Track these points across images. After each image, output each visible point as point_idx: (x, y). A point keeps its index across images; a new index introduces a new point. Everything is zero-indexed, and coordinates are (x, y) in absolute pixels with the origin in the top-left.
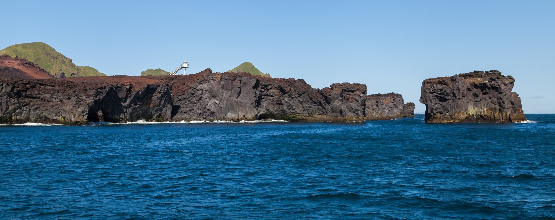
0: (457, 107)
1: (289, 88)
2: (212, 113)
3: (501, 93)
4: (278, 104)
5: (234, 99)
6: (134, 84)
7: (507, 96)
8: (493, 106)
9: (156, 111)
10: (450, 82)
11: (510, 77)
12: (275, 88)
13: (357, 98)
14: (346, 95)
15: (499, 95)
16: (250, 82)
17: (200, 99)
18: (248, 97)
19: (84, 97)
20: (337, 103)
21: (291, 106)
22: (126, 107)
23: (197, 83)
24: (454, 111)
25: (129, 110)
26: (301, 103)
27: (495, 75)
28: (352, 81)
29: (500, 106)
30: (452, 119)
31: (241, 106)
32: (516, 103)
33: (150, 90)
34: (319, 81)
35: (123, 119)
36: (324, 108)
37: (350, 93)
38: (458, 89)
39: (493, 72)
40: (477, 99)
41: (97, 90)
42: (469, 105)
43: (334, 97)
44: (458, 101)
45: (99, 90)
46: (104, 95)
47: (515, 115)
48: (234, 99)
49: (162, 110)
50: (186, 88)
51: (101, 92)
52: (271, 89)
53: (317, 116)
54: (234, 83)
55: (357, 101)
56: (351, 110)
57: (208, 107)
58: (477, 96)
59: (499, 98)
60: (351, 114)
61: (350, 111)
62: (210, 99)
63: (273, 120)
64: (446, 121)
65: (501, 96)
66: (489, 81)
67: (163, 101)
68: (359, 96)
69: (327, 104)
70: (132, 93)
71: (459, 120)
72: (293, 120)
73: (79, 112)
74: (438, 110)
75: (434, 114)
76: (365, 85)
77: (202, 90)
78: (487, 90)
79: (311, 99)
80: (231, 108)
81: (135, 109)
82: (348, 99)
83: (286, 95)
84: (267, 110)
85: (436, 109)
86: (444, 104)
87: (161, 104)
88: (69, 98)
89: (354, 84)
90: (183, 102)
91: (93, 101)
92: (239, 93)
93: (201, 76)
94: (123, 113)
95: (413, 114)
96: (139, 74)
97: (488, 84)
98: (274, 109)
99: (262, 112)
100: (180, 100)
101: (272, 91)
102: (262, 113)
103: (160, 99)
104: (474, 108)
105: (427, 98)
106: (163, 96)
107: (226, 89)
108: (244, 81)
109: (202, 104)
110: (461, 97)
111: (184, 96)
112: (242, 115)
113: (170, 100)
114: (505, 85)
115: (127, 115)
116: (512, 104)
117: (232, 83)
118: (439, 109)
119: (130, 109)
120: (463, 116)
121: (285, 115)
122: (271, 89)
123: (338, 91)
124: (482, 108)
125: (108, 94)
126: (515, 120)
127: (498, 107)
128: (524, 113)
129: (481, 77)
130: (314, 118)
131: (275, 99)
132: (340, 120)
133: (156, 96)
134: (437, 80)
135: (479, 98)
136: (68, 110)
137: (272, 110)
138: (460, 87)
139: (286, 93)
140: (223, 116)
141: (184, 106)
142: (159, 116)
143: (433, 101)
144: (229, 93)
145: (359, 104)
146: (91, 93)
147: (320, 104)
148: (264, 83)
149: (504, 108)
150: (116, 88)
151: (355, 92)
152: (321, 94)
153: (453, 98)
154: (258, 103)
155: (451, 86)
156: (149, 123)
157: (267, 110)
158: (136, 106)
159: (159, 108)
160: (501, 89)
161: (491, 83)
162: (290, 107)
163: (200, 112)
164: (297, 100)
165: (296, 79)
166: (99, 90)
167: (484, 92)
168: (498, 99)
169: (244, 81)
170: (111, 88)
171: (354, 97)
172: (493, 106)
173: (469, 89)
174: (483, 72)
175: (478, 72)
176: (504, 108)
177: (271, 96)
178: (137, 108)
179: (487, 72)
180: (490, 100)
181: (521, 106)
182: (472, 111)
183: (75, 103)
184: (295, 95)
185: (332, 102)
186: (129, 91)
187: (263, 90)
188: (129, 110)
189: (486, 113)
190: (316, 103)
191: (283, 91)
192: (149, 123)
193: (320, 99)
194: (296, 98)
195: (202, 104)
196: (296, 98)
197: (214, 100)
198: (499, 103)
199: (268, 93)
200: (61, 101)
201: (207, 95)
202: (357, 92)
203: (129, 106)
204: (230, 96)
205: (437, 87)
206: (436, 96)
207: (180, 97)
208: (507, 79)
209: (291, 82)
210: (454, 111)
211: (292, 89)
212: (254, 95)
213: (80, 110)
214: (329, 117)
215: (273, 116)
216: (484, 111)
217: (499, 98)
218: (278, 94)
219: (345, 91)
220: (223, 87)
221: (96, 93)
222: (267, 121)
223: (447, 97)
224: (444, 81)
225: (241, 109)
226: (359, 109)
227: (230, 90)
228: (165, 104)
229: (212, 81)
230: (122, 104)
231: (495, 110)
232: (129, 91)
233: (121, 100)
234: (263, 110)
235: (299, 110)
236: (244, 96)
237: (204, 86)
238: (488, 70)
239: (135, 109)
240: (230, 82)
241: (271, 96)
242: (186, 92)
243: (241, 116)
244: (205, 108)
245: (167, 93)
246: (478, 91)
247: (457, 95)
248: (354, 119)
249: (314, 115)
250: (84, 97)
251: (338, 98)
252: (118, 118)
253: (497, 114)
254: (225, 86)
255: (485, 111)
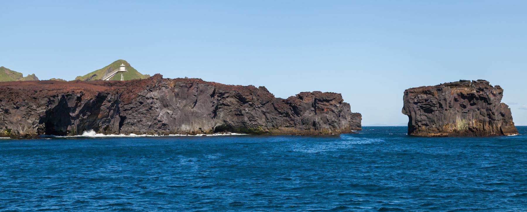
0: (445, 119)
1: (250, 97)
2: (164, 125)
3: (490, 104)
4: (236, 115)
5: (189, 109)
6: (84, 92)
7: (496, 107)
8: (482, 118)
9: (103, 123)
10: (435, 92)
11: (498, 87)
12: (232, 97)
13: (333, 109)
14: (320, 105)
15: (488, 106)
16: (207, 89)
17: (150, 109)
18: (204, 108)
19: (34, 107)
20: (308, 114)
21: (253, 117)
22: (74, 118)
23: (146, 91)
24: (441, 123)
25: (77, 122)
26: (264, 113)
27: (482, 85)
28: (191, 76)
29: (490, 118)
30: (440, 132)
31: (197, 117)
32: (506, 115)
33: (101, 98)
34: (282, 91)
35: (70, 132)
36: (292, 120)
37: (325, 103)
38: (445, 100)
39: (481, 82)
40: (465, 110)
41: (49, 99)
42: (457, 117)
43: (305, 108)
44: (444, 112)
45: (52, 99)
46: (56, 104)
47: (507, 127)
48: (189, 109)
49: (109, 122)
50: (134, 96)
51: (53, 101)
52: (227, 97)
53: (283, 128)
54: (190, 91)
55: (333, 111)
56: (327, 121)
57: (159, 119)
58: (464, 107)
59: (488, 110)
60: (327, 127)
61: (325, 123)
62: (161, 109)
63: (233, 134)
64: (433, 134)
65: (491, 107)
66: (477, 92)
67: (112, 111)
68: (335, 106)
69: (295, 115)
70: (82, 102)
71: (447, 132)
72: (255, 133)
73: (29, 123)
74: (424, 122)
75: (419, 126)
76: (340, 94)
77: (153, 99)
78: (475, 100)
79: (276, 109)
80: (186, 119)
81: (83, 120)
82: (323, 110)
83: (246, 105)
84: (225, 121)
85: (420, 121)
86: (430, 115)
87: (110, 114)
88: (18, 108)
89: (179, 78)
90: (130, 112)
91: (45, 111)
92: (196, 103)
93: (150, 82)
94: (71, 124)
95: (360, 126)
96: (73, 78)
97: (476, 94)
98: (232, 121)
99: (219, 123)
100: (126, 110)
101: (229, 99)
102: (218, 125)
103: (109, 109)
104: (462, 120)
105: (411, 109)
106: (112, 105)
107: (180, 98)
108: (201, 88)
109: (152, 115)
110: (448, 108)
111: (131, 106)
112: (198, 127)
113: (117, 111)
114: (494, 95)
115: (75, 127)
116: (503, 115)
117: (188, 91)
118: (424, 120)
119: (78, 120)
120: (450, 129)
121: (246, 127)
122: (227, 97)
123: (309, 101)
124: (470, 120)
125: (60, 102)
126: (507, 132)
127: (487, 119)
128: (516, 125)
129: (468, 86)
130: (279, 131)
131: (233, 108)
132: (313, 133)
133: (105, 105)
134: (421, 90)
135: (467, 109)
136: (15, 121)
137: (230, 122)
138: (447, 97)
139: (247, 102)
140: (176, 128)
141: (131, 117)
142: (105, 129)
143: (418, 112)
144: (184, 102)
145: (335, 115)
146: (43, 102)
147: (287, 115)
148: (221, 91)
149: (494, 120)
150: (67, 96)
151: (331, 102)
152: (287, 103)
153: (439, 109)
154: (215, 113)
155: (436, 96)
156: (108, 135)
157: (225, 121)
158: (85, 117)
159: (107, 119)
160: (490, 100)
161: (478, 94)
162: (252, 118)
163: (150, 123)
164: (259, 110)
165: (257, 86)
166: (52, 99)
167: (472, 102)
168: (487, 110)
169: (201, 88)
170: (63, 96)
171: (330, 107)
172: (482, 118)
173: (456, 100)
174: (470, 81)
175: (464, 81)
176: (494, 120)
177: (228, 105)
178: (85, 119)
179: (474, 82)
180: (478, 112)
181: (511, 118)
182: (460, 124)
183: (25, 113)
184: (257, 104)
185: (301, 113)
186: (79, 99)
187: (219, 98)
188: (77, 122)
189: (475, 126)
190: (282, 114)
191: (242, 100)
192: (108, 135)
193: (286, 108)
194: (259, 108)
195: (152, 115)
196: (259, 108)
197: (165, 110)
198: (489, 115)
199: (224, 102)
200: (7, 111)
201: (158, 104)
202: (333, 102)
203: (78, 116)
204: (185, 106)
205: (421, 97)
206: (421, 107)
207: (126, 107)
208: (495, 89)
209: (251, 89)
210: (441, 123)
211: (254, 97)
212: (211, 104)
213: (30, 121)
214: (299, 130)
215: (230, 128)
216: (473, 123)
217: (488, 110)
218: (236, 103)
219: (320, 100)
220: (177, 95)
221: (48, 102)
222: (224, 134)
223: (433, 108)
224: (429, 91)
225: (196, 120)
226: (336, 120)
227: (185, 99)
228: (113, 114)
229: (164, 88)
230: (71, 114)
231: (484, 122)
232: (79, 99)
233: (69, 110)
234: (220, 121)
235: (262, 121)
236: (201, 105)
237: (155, 94)
238: (476, 80)
239: (83, 120)
240: (186, 89)
241: (228, 105)
242: (133, 101)
243: (197, 129)
244: (155, 119)
245: (116, 102)
246: (465, 102)
247: (444, 105)
248: (330, 131)
249: (280, 128)
250: (34, 107)
251: (309, 108)
252: (64, 131)
253: (487, 127)
254: (180, 94)
255: (473, 123)
